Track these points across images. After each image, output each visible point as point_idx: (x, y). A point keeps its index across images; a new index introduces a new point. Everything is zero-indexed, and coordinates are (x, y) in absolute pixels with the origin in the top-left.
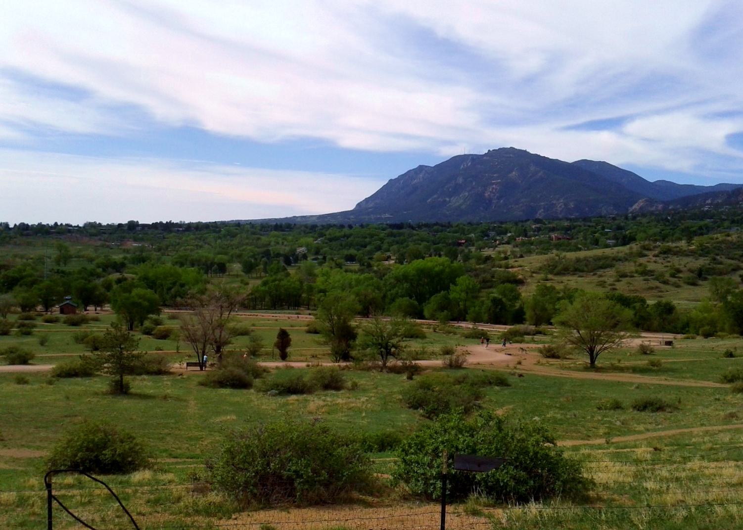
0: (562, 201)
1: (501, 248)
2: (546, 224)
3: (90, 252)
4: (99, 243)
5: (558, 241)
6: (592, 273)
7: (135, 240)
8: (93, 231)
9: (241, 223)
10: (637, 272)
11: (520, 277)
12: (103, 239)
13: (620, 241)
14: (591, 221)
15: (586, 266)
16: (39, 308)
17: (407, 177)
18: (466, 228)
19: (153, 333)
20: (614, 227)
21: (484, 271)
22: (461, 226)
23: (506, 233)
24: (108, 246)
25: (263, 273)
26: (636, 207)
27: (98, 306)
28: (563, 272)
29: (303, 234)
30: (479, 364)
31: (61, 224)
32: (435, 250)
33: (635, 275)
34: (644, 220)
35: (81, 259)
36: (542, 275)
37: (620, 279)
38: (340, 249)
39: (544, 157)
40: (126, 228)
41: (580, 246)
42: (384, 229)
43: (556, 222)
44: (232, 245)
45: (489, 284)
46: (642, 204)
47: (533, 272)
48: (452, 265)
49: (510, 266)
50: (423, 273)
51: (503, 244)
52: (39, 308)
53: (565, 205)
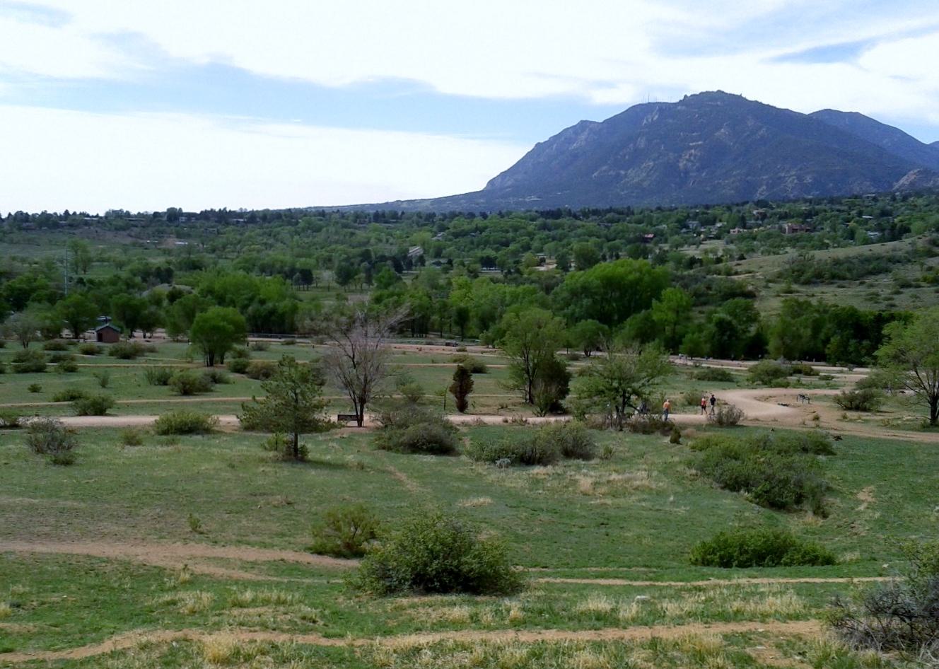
0: (794, 173)
1: (708, 245)
2: (773, 209)
3: (117, 254)
4: (128, 241)
5: (794, 234)
6: (858, 282)
7: (179, 236)
8: (120, 223)
9: (327, 212)
10: (925, 280)
11: (750, 288)
12: (133, 234)
13: (886, 232)
14: (841, 204)
15: (849, 270)
16: (66, 332)
17: (563, 139)
18: (655, 215)
19: (247, 370)
20: (877, 212)
21: (696, 280)
22: (646, 213)
23: (713, 223)
24: (141, 245)
25: (364, 285)
26: (904, 181)
27: (147, 332)
28: (814, 280)
29: (416, 227)
30: (757, 420)
31: (75, 213)
32: (611, 249)
33: (923, 284)
34: (920, 201)
35: (105, 264)
36: (784, 285)
37: (901, 290)
38: (471, 249)
39: (768, 105)
40: (165, 218)
41: (827, 241)
42: (533, 220)
43: (788, 205)
44: (314, 244)
45: (703, 299)
46: (913, 177)
47: (769, 281)
48: (653, 271)
49: (733, 272)
50: (611, 283)
51: (711, 238)
52: (66, 332)
53: (799, 178)
